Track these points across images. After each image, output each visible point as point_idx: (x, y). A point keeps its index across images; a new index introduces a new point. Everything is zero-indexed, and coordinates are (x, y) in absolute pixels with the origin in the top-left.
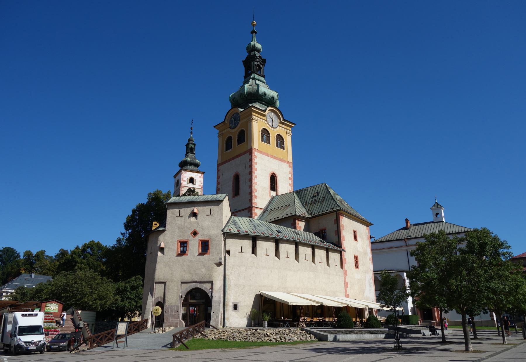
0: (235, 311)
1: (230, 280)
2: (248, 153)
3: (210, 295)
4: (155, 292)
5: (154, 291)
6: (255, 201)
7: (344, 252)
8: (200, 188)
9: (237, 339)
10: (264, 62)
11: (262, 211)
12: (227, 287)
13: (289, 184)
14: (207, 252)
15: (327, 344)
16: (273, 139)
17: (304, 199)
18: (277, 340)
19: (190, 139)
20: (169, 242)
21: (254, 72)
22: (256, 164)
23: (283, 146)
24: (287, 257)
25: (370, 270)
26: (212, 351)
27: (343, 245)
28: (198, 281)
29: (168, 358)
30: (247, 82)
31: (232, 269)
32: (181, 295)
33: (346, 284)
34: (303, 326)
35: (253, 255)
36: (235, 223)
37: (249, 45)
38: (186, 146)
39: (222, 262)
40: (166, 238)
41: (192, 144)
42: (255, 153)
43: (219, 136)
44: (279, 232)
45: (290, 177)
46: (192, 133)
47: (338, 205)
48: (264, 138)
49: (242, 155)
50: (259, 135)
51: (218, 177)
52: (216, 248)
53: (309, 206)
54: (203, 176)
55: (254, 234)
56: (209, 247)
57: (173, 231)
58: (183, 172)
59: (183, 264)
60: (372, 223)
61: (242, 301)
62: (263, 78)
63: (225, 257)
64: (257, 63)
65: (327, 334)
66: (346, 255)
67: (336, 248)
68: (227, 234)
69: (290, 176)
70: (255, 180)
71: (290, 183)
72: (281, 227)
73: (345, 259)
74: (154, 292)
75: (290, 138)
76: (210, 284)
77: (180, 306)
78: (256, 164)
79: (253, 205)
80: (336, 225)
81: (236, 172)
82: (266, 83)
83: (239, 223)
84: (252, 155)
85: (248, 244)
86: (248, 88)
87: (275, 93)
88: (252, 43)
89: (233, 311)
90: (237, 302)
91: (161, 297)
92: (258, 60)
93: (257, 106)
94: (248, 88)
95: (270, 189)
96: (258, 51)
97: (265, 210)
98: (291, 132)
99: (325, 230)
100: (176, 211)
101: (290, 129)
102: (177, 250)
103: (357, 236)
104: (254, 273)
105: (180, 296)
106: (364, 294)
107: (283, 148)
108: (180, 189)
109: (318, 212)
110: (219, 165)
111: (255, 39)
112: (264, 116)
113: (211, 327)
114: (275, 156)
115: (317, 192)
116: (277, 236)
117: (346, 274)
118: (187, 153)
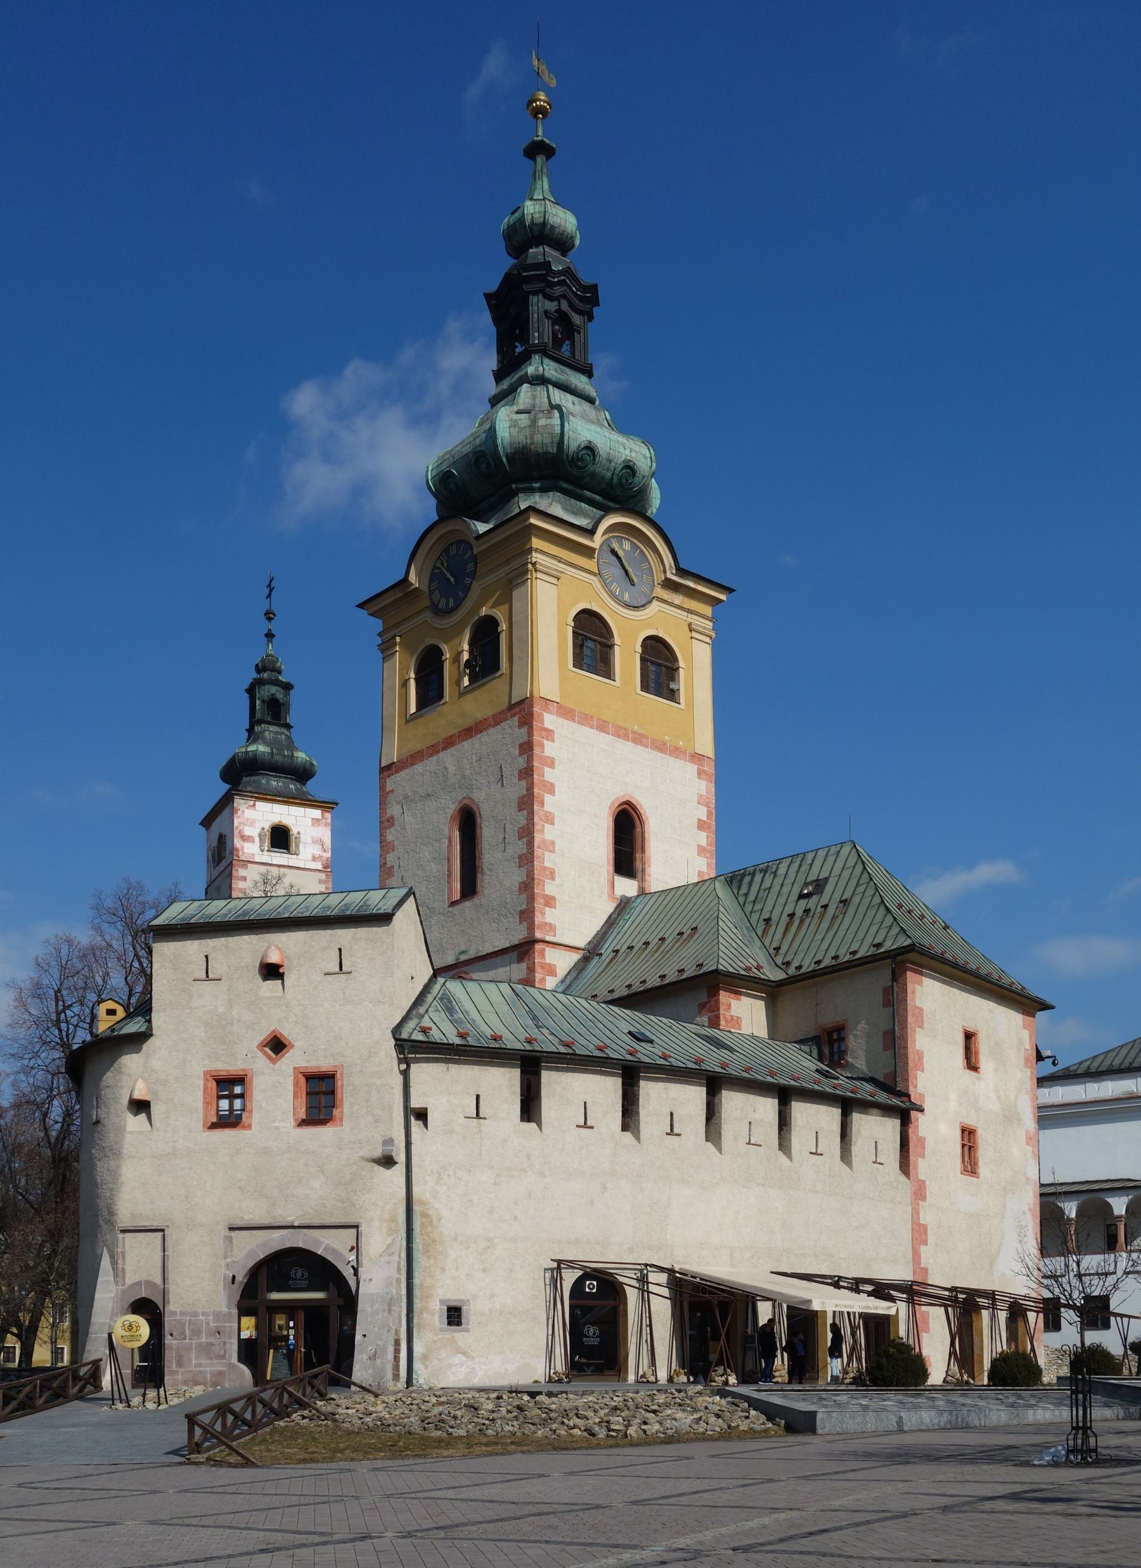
1: (431, 1221)
3: (348, 1273)
6: (546, 916)
7: (919, 1115)
8: (320, 867)
9: (452, 1427)
10: (590, 297)
11: (575, 957)
15: (806, 1444)
17: (758, 907)
18: (614, 1430)
23: (672, 686)
24: (672, 1132)
25: (1028, 1179)
26: (342, 1470)
27: (915, 1087)
29: (156, 1492)
34: (726, 1383)
36: (448, 1005)
37: (517, 215)
38: (248, 691)
40: (155, 1063)
41: (277, 683)
42: (550, 720)
44: (638, 1039)
45: (705, 818)
46: (273, 636)
48: (586, 652)
49: (486, 729)
52: (368, 1101)
54: (329, 821)
55: (528, 1047)
58: (239, 802)
60: (1048, 998)
62: (584, 378)
64: (556, 303)
65: (812, 1408)
66: (922, 1124)
67: (882, 1097)
69: (702, 812)
70: (545, 833)
71: (704, 843)
72: (652, 1018)
73: (922, 1141)
75: (707, 650)
82: (597, 403)
83: (468, 1006)
85: (768, 1106)
86: (514, 426)
87: (637, 449)
90: (462, 1297)
91: (149, 1284)
93: (557, 510)
94: (514, 424)
95: (611, 868)
96: (563, 244)
97: (591, 953)
98: (711, 624)
100: (193, 949)
101: (707, 610)
103: (977, 1053)
106: (991, 1267)
107: (672, 695)
108: (230, 875)
109: (814, 961)
111: (546, 186)
112: (588, 552)
113: (353, 1388)
114: (634, 732)
115: (817, 880)
116: (631, 1054)
117: (920, 1193)
118: (254, 722)
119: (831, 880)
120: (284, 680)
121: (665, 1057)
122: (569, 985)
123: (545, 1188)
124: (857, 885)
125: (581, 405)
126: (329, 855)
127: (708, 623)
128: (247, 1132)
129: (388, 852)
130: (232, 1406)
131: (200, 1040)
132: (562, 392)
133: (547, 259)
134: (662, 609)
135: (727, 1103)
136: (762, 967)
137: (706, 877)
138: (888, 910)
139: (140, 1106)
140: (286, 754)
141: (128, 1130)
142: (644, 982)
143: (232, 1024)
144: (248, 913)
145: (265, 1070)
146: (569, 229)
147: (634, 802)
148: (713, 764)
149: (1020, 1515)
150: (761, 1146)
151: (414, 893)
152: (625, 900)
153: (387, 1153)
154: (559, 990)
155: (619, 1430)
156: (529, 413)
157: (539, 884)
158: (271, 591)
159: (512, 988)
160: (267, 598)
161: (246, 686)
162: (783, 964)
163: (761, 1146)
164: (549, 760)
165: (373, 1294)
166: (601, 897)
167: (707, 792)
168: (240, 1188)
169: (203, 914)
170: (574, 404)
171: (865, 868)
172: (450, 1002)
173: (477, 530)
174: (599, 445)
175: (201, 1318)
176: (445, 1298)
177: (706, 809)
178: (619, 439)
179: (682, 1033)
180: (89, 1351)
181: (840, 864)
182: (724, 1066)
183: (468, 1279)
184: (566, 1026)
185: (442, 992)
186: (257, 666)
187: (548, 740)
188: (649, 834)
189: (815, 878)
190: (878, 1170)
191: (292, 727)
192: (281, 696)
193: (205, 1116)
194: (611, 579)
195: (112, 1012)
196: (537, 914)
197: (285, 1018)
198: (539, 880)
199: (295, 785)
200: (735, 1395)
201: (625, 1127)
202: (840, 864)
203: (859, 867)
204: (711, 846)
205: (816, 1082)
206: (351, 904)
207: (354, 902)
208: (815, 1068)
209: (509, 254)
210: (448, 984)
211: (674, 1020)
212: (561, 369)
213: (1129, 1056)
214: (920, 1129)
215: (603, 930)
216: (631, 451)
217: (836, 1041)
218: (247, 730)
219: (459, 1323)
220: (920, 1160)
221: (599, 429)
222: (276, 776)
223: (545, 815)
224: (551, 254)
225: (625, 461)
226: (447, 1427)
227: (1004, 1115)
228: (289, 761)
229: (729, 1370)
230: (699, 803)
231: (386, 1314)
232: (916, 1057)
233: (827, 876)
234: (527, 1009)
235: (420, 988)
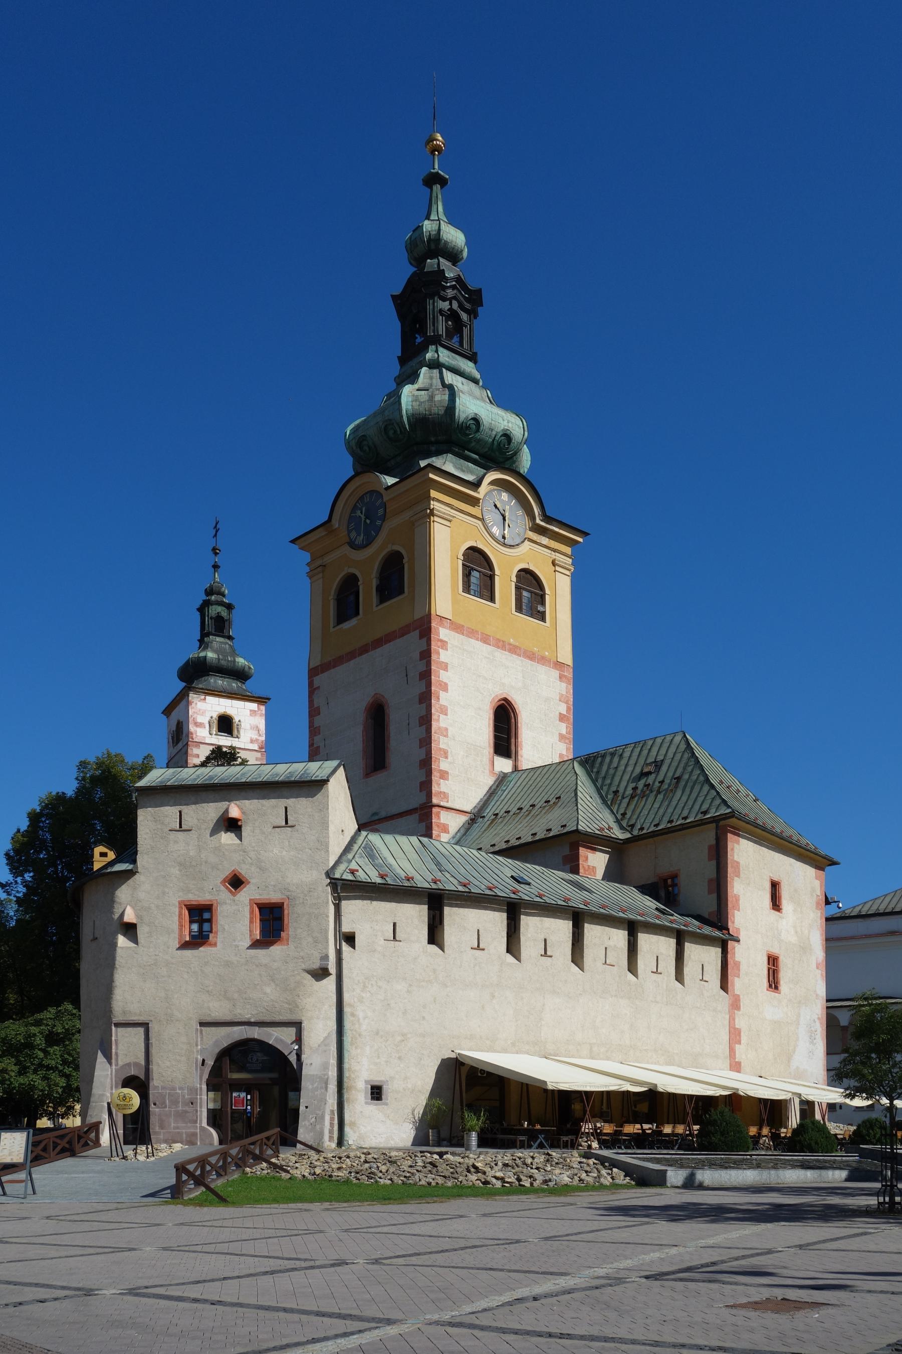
1: (359, 1020)
2: (415, 630)
3: (293, 1058)
4: (117, 1049)
5: (114, 1047)
6: (439, 786)
7: (736, 944)
8: (256, 748)
9: (380, 1178)
10: (475, 299)
11: (463, 819)
12: (347, 1039)
18: (508, 1182)
19: (211, 587)
20: (152, 905)
21: (436, 341)
23: (540, 608)
27: (733, 923)
30: (412, 377)
31: (365, 986)
32: (200, 1059)
33: (735, 1035)
34: (590, 1147)
35: (434, 948)
36: (370, 853)
37: (417, 233)
38: (198, 610)
39: (329, 967)
40: (142, 895)
42: (442, 633)
43: (311, 575)
44: (519, 882)
47: (724, 802)
50: (454, 570)
51: (314, 712)
52: (308, 926)
53: (624, 804)
55: (434, 886)
58: (192, 696)
60: (836, 859)
61: (397, 1076)
62: (471, 364)
63: (339, 953)
66: (738, 952)
69: (563, 708)
70: (439, 722)
71: (564, 732)
73: (737, 965)
74: (114, 1051)
76: (292, 1031)
77: (201, 1088)
79: (435, 801)
80: (714, 862)
81: (373, 694)
82: (481, 384)
83: (385, 853)
86: (416, 401)
87: (513, 421)
90: (383, 1079)
91: (136, 1065)
93: (449, 468)
94: (416, 399)
95: (492, 750)
96: (453, 256)
97: (475, 817)
98: (571, 560)
99: (674, 877)
100: (170, 813)
101: (568, 550)
103: (780, 898)
105: (196, 1063)
106: (789, 1062)
107: (542, 617)
108: (186, 753)
109: (653, 824)
110: (313, 672)
112: (474, 502)
114: (510, 644)
115: (655, 762)
116: (514, 893)
117: (735, 1005)
118: (204, 634)
120: (227, 602)
121: (540, 896)
122: (462, 838)
123: (447, 995)
125: (468, 385)
126: (263, 738)
127: (568, 559)
128: (214, 949)
129: (315, 736)
131: (176, 877)
132: (453, 374)
133: (441, 268)
134: (531, 547)
135: (588, 932)
136: (612, 829)
137: (566, 759)
139: (130, 930)
140: (230, 659)
141: (119, 945)
142: (519, 838)
143: (201, 864)
144: (213, 778)
145: (227, 901)
146: (460, 244)
147: (510, 699)
148: (572, 670)
149: (606, 1231)
150: (614, 966)
152: (502, 776)
153: (324, 966)
155: (512, 1182)
156: (428, 390)
157: (435, 761)
158: (217, 532)
159: (420, 841)
160: (214, 537)
161: (198, 606)
162: (629, 826)
163: (614, 966)
164: (443, 665)
165: (313, 1075)
166: (484, 772)
167: (567, 692)
168: (208, 991)
169: (177, 778)
170: (463, 384)
172: (372, 850)
173: (387, 483)
174: (483, 417)
175: (178, 1091)
176: (369, 1079)
177: (565, 705)
178: (499, 412)
179: (552, 878)
180: (91, 1116)
181: (673, 749)
183: (387, 1065)
184: (462, 871)
185: (365, 843)
186: (206, 590)
187: (442, 648)
188: (521, 724)
189: (653, 760)
190: (704, 986)
191: (234, 639)
192: (226, 614)
193: (181, 935)
194: (492, 523)
195: (103, 855)
197: (243, 861)
198: (436, 758)
199: (237, 684)
200: (598, 1157)
202: (673, 749)
204: (570, 734)
205: (658, 918)
206: (294, 772)
207: (297, 771)
208: (655, 907)
209: (411, 264)
211: (545, 867)
212: (452, 356)
213: (892, 902)
214: (736, 955)
215: (486, 798)
216: (508, 422)
217: (671, 886)
218: (198, 640)
220: (736, 979)
221: (483, 404)
222: (222, 677)
224: (444, 263)
225: (503, 430)
226: (377, 1178)
227: (800, 946)
228: (232, 665)
229: (592, 1137)
230: (560, 701)
231: (323, 1091)
232: (734, 899)
233: (662, 759)
234: (432, 857)
235: (348, 839)
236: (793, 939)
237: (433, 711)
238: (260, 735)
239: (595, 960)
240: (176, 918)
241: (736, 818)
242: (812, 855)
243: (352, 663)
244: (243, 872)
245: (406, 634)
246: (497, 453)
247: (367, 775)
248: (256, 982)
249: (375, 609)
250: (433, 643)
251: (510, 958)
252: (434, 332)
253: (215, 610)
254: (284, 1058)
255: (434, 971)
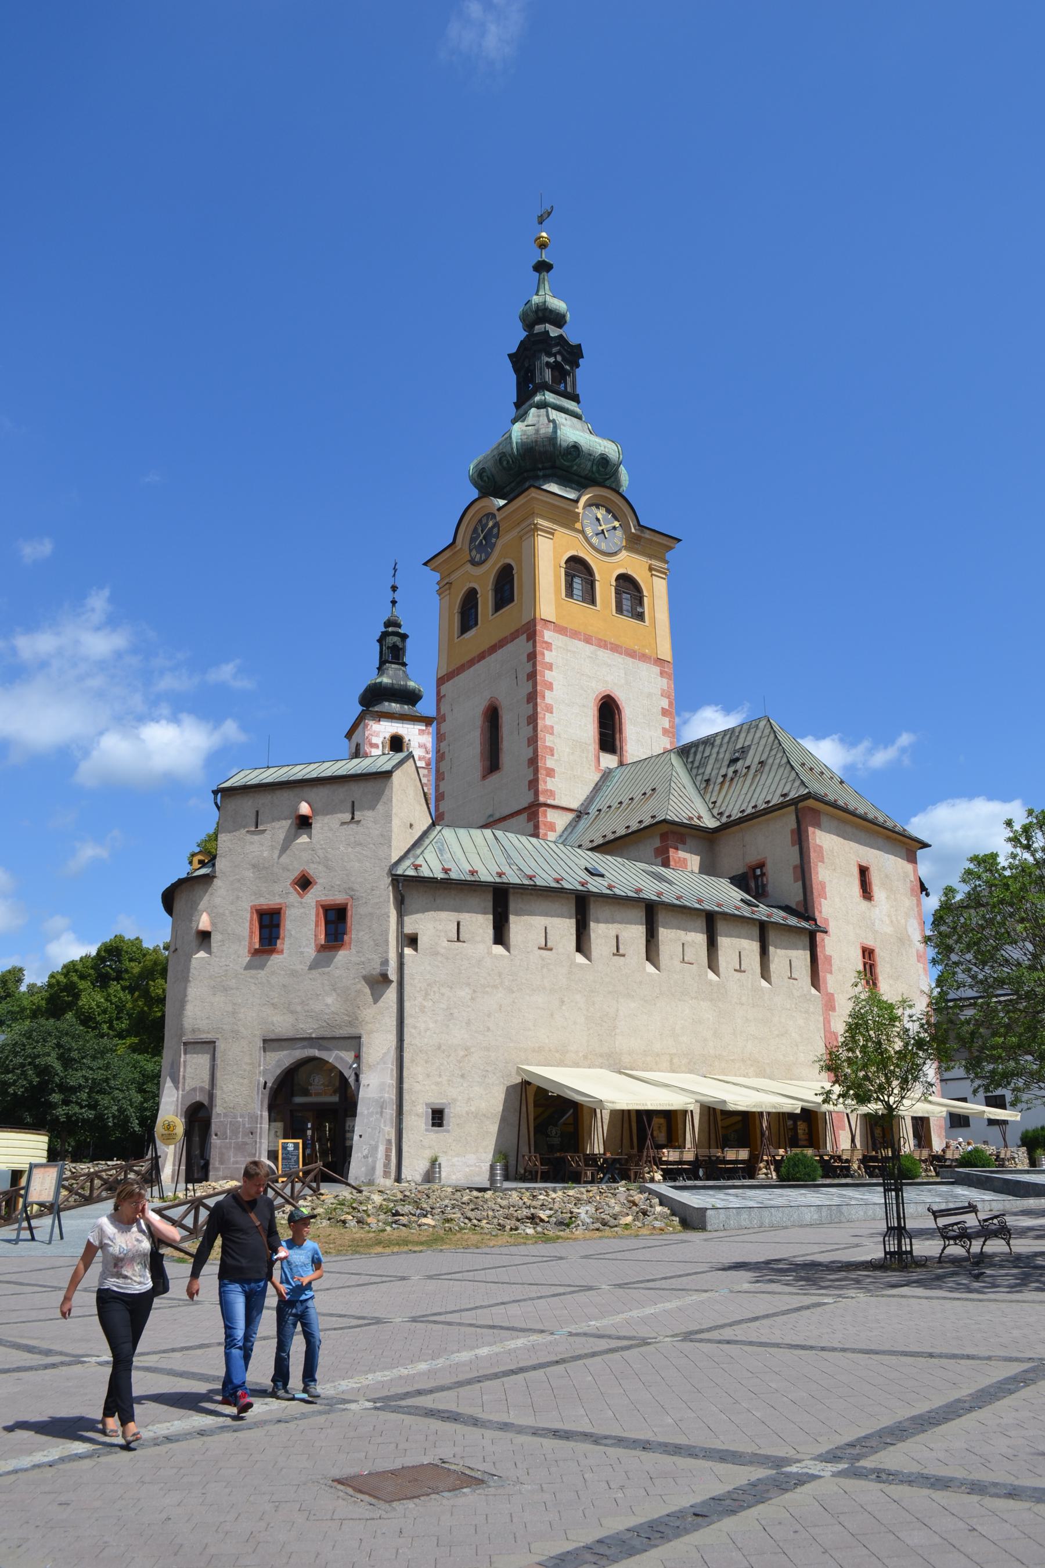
0: (437, 1132)
4: (185, 1071)
5: (182, 1069)
6: (547, 784)
11: (571, 816)
13: (663, 728)
14: (342, 940)
16: (605, 589)
17: (701, 771)
19: (389, 620)
20: (227, 912)
21: (544, 387)
22: (550, 668)
23: (639, 610)
24: (618, 953)
27: (821, 912)
28: (314, 1036)
30: (520, 417)
31: (427, 994)
32: (262, 1080)
35: (499, 949)
37: (528, 305)
38: (378, 641)
39: (389, 973)
42: (548, 635)
43: (440, 593)
44: (592, 874)
45: (667, 707)
46: (396, 602)
47: (803, 783)
50: (557, 577)
53: (715, 794)
55: (498, 880)
56: (349, 924)
57: (237, 877)
59: (268, 981)
61: (460, 1098)
63: (401, 956)
67: (793, 921)
68: (405, 880)
69: (665, 703)
70: (546, 720)
72: (609, 857)
73: (829, 959)
74: (181, 1074)
77: (261, 1115)
78: (550, 668)
80: (797, 847)
81: (489, 697)
84: (535, 642)
87: (609, 446)
88: (536, 299)
89: (432, 1131)
90: (444, 1101)
91: (202, 1089)
92: (554, 350)
95: (597, 746)
96: (559, 320)
97: (580, 814)
99: (762, 865)
102: (251, 937)
103: (870, 884)
104: (501, 1006)
105: (258, 1084)
107: (640, 617)
114: (611, 643)
115: (743, 748)
118: (383, 662)
119: (752, 747)
123: (514, 1002)
124: (771, 750)
130: (205, 1201)
138: (792, 768)
143: (273, 866)
151: (413, 756)
153: (384, 972)
154: (560, 841)
161: (378, 638)
165: (370, 1098)
168: (273, 1004)
171: (776, 737)
172: (443, 845)
179: (632, 870)
182: (659, 894)
184: (533, 864)
193: (250, 943)
196: (541, 782)
201: (579, 949)
202: (758, 735)
203: (772, 736)
210: (443, 832)
219: (440, 1125)
220: (828, 976)
223: (546, 706)
230: (662, 696)
231: (378, 1116)
232: (820, 886)
236: (889, 930)
237: (539, 710)
238: (427, 753)
239: (672, 959)
240: (247, 924)
241: (813, 798)
242: (890, 833)
243: (472, 669)
244: (311, 873)
245: (516, 638)
246: (597, 475)
247: (484, 777)
248: (319, 993)
249: (491, 618)
250: (538, 645)
251: (580, 959)
252: (541, 379)
253: (392, 640)
254: (344, 1080)
255: (500, 974)
